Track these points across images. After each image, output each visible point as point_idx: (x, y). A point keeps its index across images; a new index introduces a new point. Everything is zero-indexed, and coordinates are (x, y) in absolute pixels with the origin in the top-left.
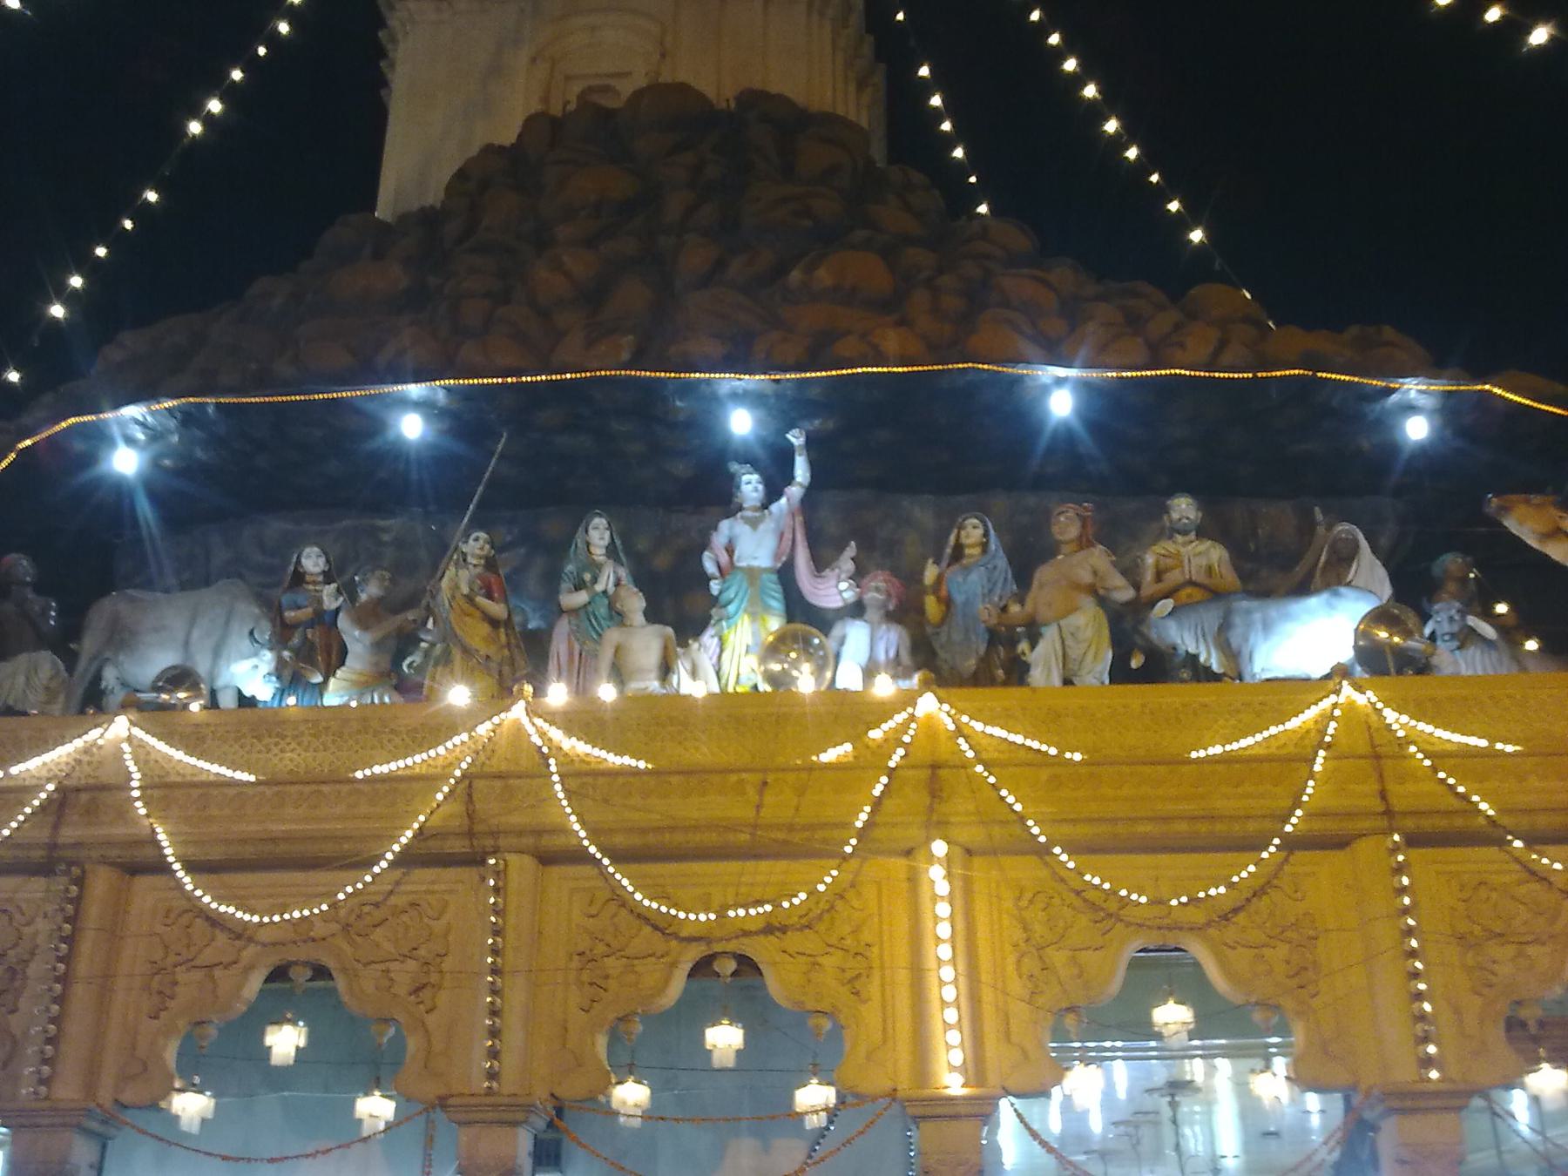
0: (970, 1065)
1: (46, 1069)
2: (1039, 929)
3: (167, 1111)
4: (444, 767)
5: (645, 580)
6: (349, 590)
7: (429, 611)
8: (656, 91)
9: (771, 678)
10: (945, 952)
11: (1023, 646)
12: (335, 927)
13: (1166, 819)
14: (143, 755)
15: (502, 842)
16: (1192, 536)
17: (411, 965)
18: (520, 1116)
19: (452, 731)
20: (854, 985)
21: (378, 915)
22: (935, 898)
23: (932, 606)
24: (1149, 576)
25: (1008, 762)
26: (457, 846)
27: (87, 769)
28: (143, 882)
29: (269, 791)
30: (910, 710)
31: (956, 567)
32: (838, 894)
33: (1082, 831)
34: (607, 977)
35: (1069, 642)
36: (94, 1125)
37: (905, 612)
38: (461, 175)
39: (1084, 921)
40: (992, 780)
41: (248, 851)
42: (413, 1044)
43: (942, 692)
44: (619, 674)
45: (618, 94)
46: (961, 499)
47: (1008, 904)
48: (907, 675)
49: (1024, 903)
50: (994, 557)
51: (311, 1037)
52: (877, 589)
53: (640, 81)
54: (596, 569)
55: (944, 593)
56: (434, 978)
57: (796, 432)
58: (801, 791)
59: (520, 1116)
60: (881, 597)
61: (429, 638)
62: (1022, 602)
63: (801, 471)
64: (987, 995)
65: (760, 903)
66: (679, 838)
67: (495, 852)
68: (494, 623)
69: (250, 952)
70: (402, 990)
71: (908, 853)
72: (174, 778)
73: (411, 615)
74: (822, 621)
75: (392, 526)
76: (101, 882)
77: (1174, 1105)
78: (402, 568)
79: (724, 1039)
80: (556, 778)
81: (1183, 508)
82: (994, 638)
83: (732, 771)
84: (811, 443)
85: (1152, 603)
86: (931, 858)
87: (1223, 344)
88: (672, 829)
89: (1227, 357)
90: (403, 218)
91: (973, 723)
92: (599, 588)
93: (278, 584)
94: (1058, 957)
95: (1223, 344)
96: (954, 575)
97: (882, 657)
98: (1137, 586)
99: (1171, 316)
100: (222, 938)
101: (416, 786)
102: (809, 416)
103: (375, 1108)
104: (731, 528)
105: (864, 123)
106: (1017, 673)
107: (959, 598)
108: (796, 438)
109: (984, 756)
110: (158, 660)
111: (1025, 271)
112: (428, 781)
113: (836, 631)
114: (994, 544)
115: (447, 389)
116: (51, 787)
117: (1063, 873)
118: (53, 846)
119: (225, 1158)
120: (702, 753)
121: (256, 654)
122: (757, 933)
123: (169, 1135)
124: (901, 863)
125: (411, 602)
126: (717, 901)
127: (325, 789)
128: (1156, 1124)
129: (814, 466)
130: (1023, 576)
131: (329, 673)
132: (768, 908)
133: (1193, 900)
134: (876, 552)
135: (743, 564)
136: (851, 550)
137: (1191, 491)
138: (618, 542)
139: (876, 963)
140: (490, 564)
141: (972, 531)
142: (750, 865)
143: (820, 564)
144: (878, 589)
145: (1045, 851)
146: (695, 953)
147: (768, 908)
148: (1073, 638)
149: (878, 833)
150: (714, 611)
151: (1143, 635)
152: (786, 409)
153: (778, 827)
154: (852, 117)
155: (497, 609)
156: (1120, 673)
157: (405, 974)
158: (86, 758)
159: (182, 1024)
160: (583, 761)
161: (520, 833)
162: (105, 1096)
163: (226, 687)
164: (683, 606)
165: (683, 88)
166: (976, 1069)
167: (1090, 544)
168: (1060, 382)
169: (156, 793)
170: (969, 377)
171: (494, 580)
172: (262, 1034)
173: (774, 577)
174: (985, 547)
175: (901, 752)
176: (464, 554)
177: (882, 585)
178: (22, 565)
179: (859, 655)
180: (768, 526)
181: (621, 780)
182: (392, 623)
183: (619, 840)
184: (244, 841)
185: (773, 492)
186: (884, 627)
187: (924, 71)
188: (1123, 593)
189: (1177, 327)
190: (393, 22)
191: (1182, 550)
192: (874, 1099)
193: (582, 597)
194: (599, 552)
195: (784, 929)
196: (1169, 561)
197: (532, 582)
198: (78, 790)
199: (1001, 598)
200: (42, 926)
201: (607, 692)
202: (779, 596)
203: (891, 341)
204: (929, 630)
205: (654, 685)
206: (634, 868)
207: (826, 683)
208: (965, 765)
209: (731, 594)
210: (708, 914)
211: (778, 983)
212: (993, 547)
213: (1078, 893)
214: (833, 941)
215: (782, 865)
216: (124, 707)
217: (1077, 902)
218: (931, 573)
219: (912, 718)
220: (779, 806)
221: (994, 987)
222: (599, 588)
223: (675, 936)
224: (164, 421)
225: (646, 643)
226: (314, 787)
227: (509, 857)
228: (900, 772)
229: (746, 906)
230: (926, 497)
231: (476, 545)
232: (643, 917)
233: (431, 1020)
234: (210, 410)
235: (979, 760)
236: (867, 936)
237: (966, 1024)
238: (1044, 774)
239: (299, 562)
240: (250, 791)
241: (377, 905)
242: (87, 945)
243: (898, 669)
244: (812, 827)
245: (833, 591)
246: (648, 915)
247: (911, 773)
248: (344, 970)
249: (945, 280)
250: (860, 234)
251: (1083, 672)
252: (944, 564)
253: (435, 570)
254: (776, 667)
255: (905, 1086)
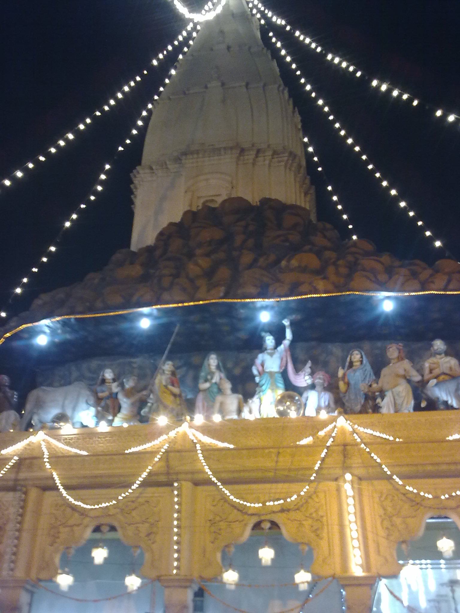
0: (364, 564)
1: (12, 565)
2: (389, 509)
3: (55, 582)
4: (158, 448)
5: (231, 377)
6: (122, 385)
7: (151, 391)
8: (230, 200)
9: (280, 413)
10: (352, 518)
11: (379, 400)
12: (118, 510)
13: (438, 464)
14: (49, 447)
15: (181, 476)
16: (443, 355)
17: (147, 525)
18: (188, 584)
19: (160, 434)
20: (317, 532)
21: (134, 505)
22: (347, 497)
23: (342, 386)
24: (427, 371)
25: (375, 443)
26: (163, 478)
27: (28, 451)
28: (48, 493)
29: (94, 458)
30: (334, 423)
31: (350, 370)
32: (309, 496)
33: (405, 470)
34: (220, 529)
35: (396, 397)
36: (29, 587)
37: (331, 387)
38: (161, 234)
39: (407, 506)
40: (368, 450)
41: (86, 481)
42: (147, 556)
43: (346, 416)
44: (222, 411)
45: (216, 202)
46: (352, 344)
47: (377, 500)
48: (333, 411)
49: (382, 499)
50: (365, 366)
51: (110, 553)
52: (320, 378)
53: (224, 197)
54: (212, 374)
55: (346, 380)
56: (155, 529)
57: (286, 320)
58: (293, 456)
59: (188, 584)
60: (321, 381)
61: (151, 401)
62: (377, 383)
63: (289, 334)
64: (370, 536)
65: (278, 499)
66: (246, 475)
67: (176, 481)
68: (175, 395)
69: (86, 521)
70: (142, 535)
71: (336, 479)
72: (61, 455)
73: (145, 393)
74: (300, 391)
75: (138, 361)
76: (33, 493)
77: (453, 591)
78: (141, 377)
79: (267, 554)
80: (199, 452)
81: (439, 344)
82: (367, 397)
83: (267, 448)
84: (292, 324)
85: (428, 382)
86: (345, 481)
87: (449, 282)
88: (244, 471)
89: (451, 286)
90: (141, 250)
91: (359, 428)
92: (214, 381)
93: (96, 384)
94: (398, 521)
95: (449, 282)
96: (350, 372)
97: (323, 405)
98: (423, 376)
99: (429, 272)
100: (76, 515)
101: (147, 455)
102: (291, 314)
103: (133, 582)
104: (263, 357)
105: (308, 208)
106: (376, 409)
107: (352, 382)
108: (286, 322)
109: (364, 441)
110: (54, 412)
111: (372, 257)
112: (152, 453)
113: (305, 395)
114: (365, 361)
115: (157, 309)
116: (16, 458)
117: (398, 487)
118: (16, 480)
119: (77, 600)
120: (253, 442)
121: (88, 409)
122: (277, 512)
123: (56, 591)
124: (333, 484)
125: (145, 388)
126: (262, 500)
127: (114, 457)
128: (447, 601)
129: (294, 333)
130: (377, 374)
131: (115, 415)
132: (282, 501)
133: (451, 496)
134: (318, 364)
135: (267, 370)
136: (309, 364)
137: (443, 338)
138: (220, 364)
139: (325, 523)
140: (173, 374)
141: (356, 356)
142: (274, 486)
143: (297, 370)
144: (320, 378)
145: (390, 478)
146: (254, 520)
147: (282, 501)
148: (397, 395)
149: (325, 472)
150: (257, 389)
151: (426, 395)
152: (283, 312)
153: (284, 470)
154: (303, 205)
155: (176, 390)
156: (417, 408)
157: (144, 528)
158: (28, 447)
159: (62, 548)
160: (209, 446)
161: (187, 473)
162: (33, 576)
163: (77, 422)
164: (245, 386)
165: (240, 199)
166: (367, 566)
167: (402, 359)
168: (388, 298)
169: (53, 460)
170: (351, 297)
171: (175, 379)
172: (90, 552)
173: (280, 375)
174: (362, 362)
175: (332, 439)
176: (164, 370)
177: (321, 377)
178: (5, 379)
179: (315, 402)
180: (277, 356)
181: (224, 452)
182: (137, 396)
183: (224, 475)
184: (85, 477)
185: (278, 343)
186: (323, 393)
187: (330, 188)
188: (417, 378)
189: (431, 276)
190: (136, 181)
191: (440, 361)
192: (326, 578)
193: (207, 385)
194: (213, 368)
195: (288, 510)
196: (435, 366)
197: (189, 380)
198: (26, 459)
199: (369, 382)
200: (12, 510)
201: (217, 418)
202: (282, 382)
203: (321, 284)
204: (341, 395)
205: (235, 417)
206: (230, 487)
207: (301, 415)
208: (357, 444)
209: (263, 382)
210: (260, 508)
211: (287, 532)
212: (364, 362)
213: (404, 495)
214: (308, 515)
215: (286, 485)
216: (42, 428)
217: (404, 498)
218: (341, 373)
219: (335, 427)
220: (285, 462)
221: (373, 532)
222: (214, 381)
223: (246, 513)
224: (56, 325)
225: (232, 401)
226: (110, 457)
227: (184, 483)
228: (331, 448)
229: (274, 501)
230: (337, 344)
231: (168, 366)
232: (234, 506)
233: (154, 546)
234: (72, 320)
235: (362, 442)
236: (321, 513)
237: (361, 538)
238: (388, 447)
239: (103, 375)
240: (87, 458)
241: (133, 502)
242: (28, 518)
243: (329, 409)
244: (297, 470)
245: (302, 380)
246: (236, 505)
247: (335, 448)
248: (122, 527)
249: (340, 262)
250: (307, 247)
251: (403, 409)
252: (346, 369)
253: (153, 376)
254: (281, 408)
255: (338, 571)
